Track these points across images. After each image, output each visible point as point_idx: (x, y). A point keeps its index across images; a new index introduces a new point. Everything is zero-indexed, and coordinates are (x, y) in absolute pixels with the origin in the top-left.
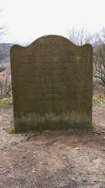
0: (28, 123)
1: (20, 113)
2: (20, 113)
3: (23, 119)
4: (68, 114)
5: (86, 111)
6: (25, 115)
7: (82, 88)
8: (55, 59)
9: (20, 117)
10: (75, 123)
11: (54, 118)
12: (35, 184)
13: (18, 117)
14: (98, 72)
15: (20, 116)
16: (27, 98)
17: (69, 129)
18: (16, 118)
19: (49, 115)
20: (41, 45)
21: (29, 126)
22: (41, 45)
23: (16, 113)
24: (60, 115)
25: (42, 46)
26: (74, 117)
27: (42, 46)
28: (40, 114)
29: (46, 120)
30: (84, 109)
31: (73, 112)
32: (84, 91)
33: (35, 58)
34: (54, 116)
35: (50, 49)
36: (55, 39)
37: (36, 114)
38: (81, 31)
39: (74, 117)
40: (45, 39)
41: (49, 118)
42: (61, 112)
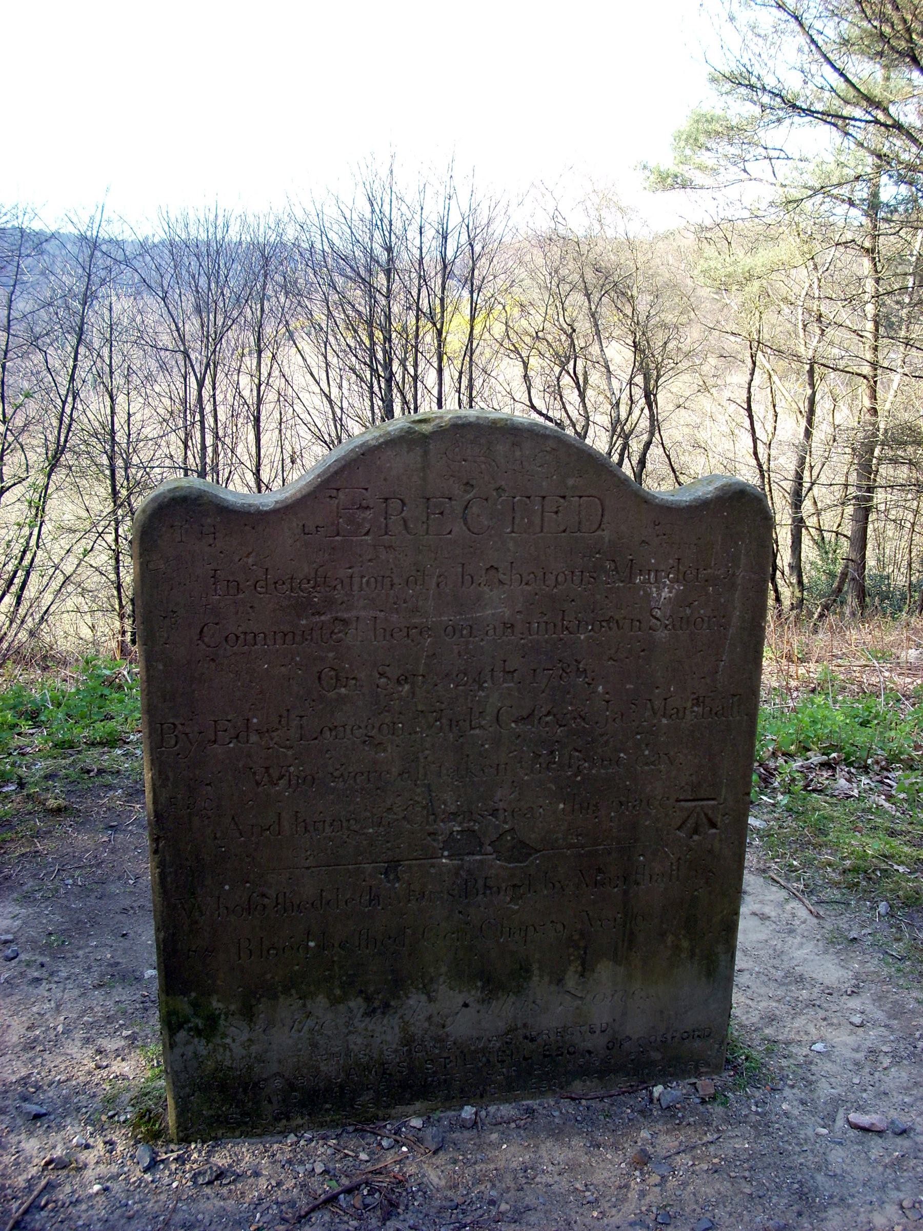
0: (274, 1068)
1: (215, 1004)
2: (215, 1004)
3: (237, 1042)
4: (571, 981)
5: (692, 955)
6: (248, 1013)
7: (678, 801)
8: (497, 604)
9: (210, 1028)
10: (614, 1044)
11: (459, 1015)
12: (895, 1003)
13: (199, 1033)
14: (803, 670)
15: (212, 1021)
16: (264, 895)
17: (569, 1083)
18: (182, 1035)
19: (430, 1000)
20: (386, 499)
21: (278, 1083)
22: (386, 499)
23: (183, 1005)
24: (512, 998)
25: (395, 504)
26: (604, 1003)
27: (395, 504)
28: (368, 999)
29: (408, 1041)
30: (685, 944)
31: (605, 971)
32: (691, 821)
33: (339, 595)
34: (466, 1005)
35: (458, 528)
36: (501, 448)
37: (335, 1001)
38: (384, 173)
39: (604, 1003)
40: (419, 451)
41: (430, 1018)
42: (523, 970)
